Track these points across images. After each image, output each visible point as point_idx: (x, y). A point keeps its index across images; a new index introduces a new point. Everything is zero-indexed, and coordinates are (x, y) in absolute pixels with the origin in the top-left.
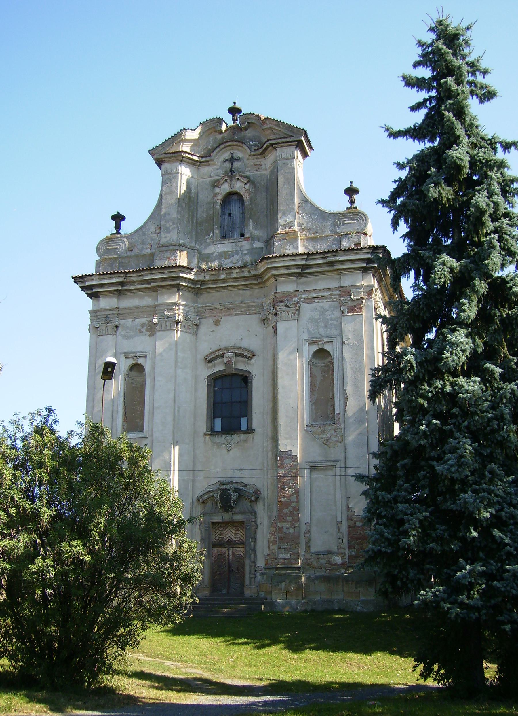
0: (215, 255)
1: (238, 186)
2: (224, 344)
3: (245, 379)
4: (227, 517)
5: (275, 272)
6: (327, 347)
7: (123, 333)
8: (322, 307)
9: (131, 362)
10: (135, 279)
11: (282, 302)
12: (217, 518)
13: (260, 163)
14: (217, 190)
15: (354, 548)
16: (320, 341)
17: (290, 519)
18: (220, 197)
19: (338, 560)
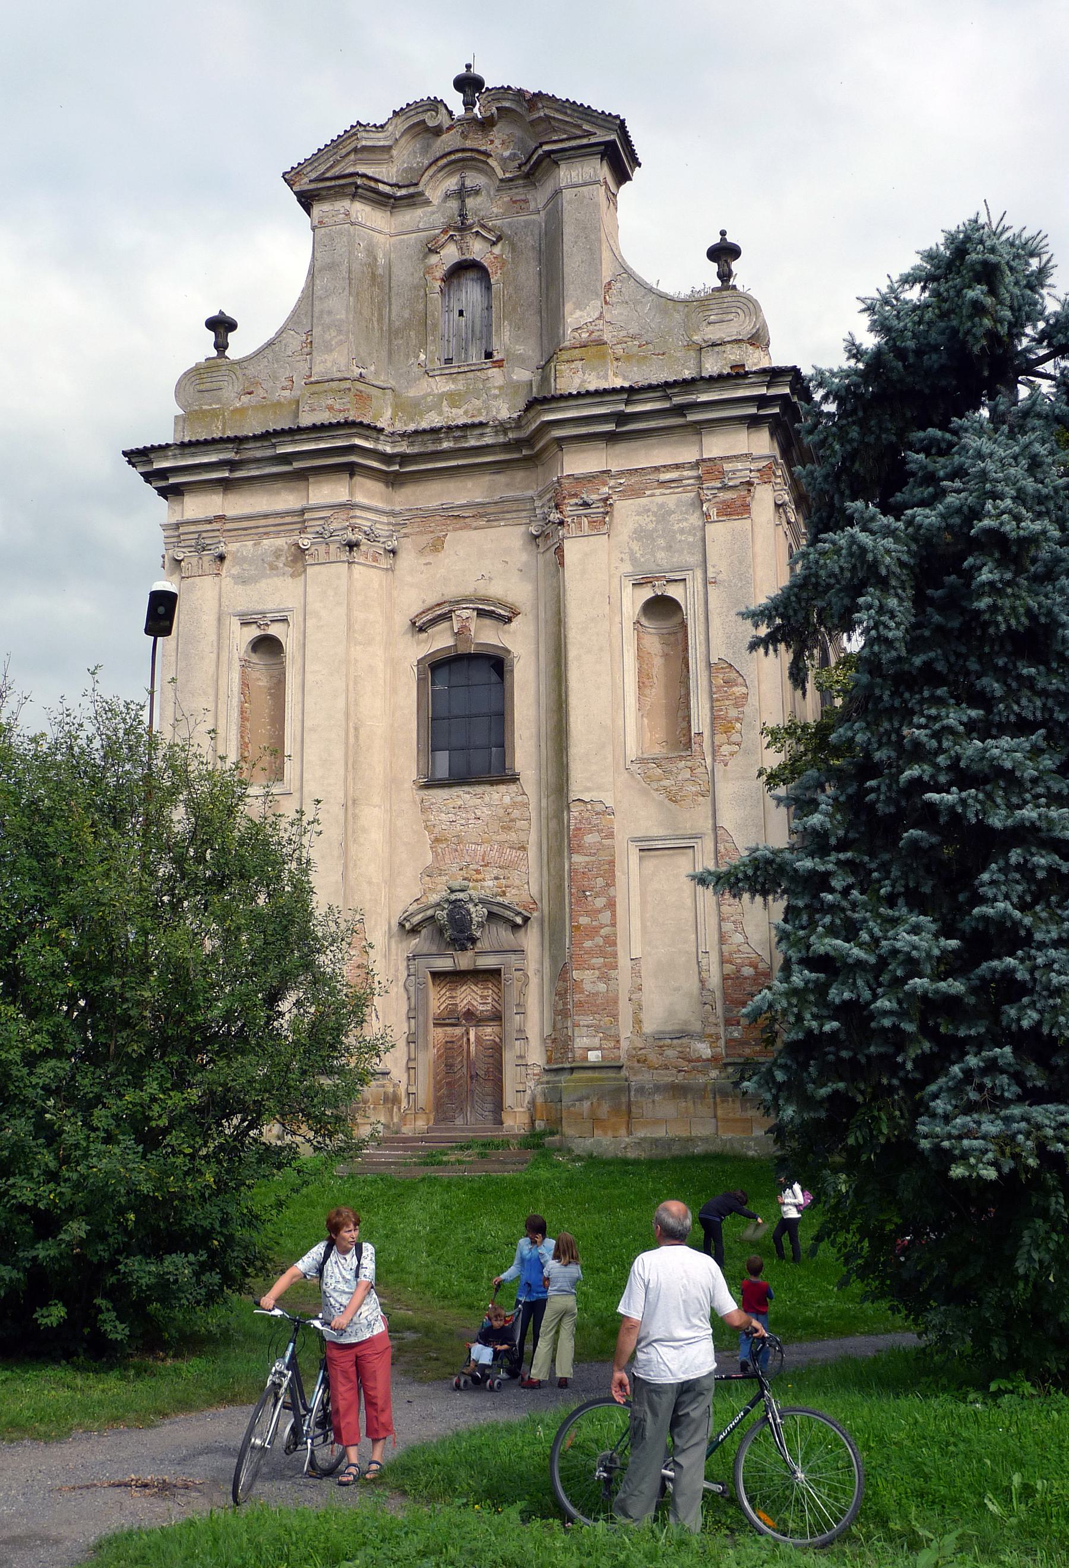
0: (430, 399)
1: (477, 250)
2: (452, 591)
3: (497, 664)
4: (464, 961)
5: (558, 433)
6: (674, 592)
7: (235, 571)
8: (661, 506)
9: (254, 632)
10: (259, 454)
11: (575, 495)
12: (444, 964)
13: (523, 197)
14: (434, 259)
15: (738, 1024)
16: (658, 579)
17: (598, 961)
18: (439, 273)
19: (705, 1050)
